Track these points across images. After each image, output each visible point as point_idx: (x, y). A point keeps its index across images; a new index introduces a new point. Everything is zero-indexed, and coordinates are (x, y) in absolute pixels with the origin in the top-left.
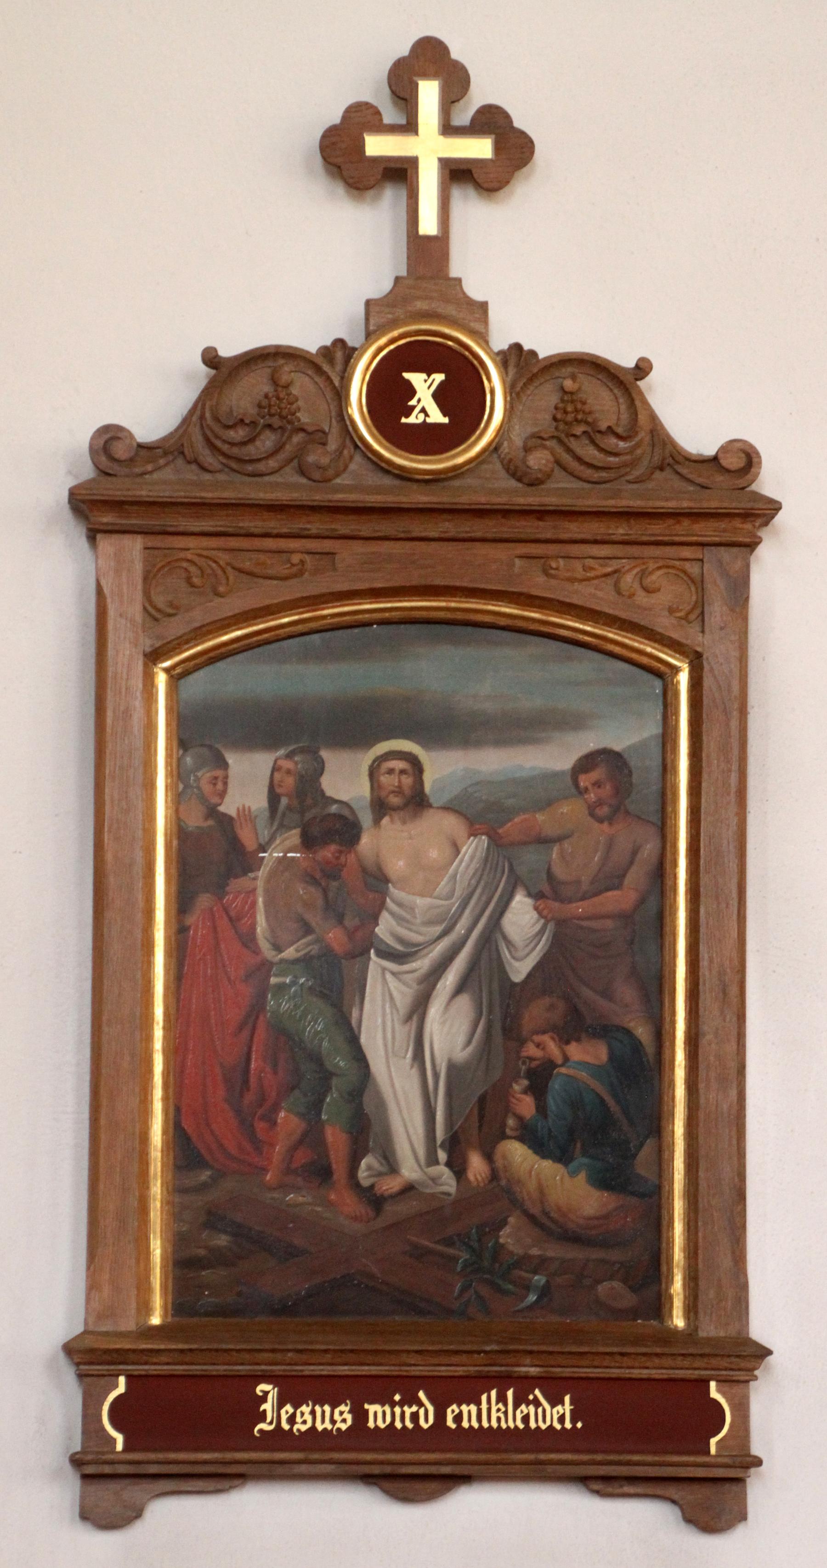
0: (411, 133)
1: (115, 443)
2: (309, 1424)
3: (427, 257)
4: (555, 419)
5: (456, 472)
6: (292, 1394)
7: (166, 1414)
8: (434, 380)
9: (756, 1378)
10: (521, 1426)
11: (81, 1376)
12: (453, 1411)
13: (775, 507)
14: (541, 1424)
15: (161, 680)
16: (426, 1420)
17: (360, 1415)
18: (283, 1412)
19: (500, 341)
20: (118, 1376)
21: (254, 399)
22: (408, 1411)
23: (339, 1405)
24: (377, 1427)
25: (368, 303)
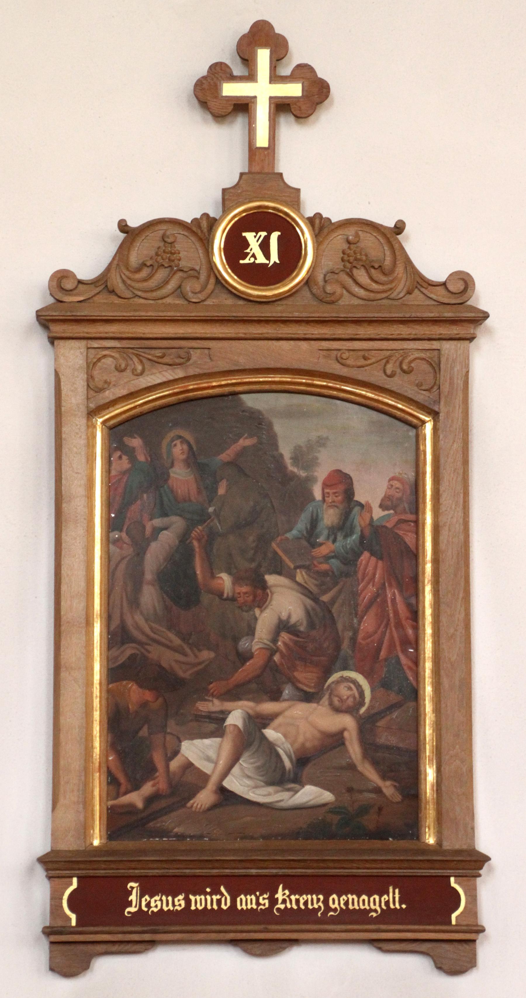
0: (253, 80)
1: (64, 281)
4: (343, 260)
6: (149, 888)
7: (99, 902)
8: (260, 236)
9: (480, 876)
10: (295, 907)
11: (49, 878)
12: (385, 899)
13: (485, 316)
16: (226, 904)
17: (188, 902)
18: (143, 900)
19: (310, 213)
20: (71, 877)
21: (152, 248)
22: (215, 898)
24: (197, 909)
25: (224, 191)
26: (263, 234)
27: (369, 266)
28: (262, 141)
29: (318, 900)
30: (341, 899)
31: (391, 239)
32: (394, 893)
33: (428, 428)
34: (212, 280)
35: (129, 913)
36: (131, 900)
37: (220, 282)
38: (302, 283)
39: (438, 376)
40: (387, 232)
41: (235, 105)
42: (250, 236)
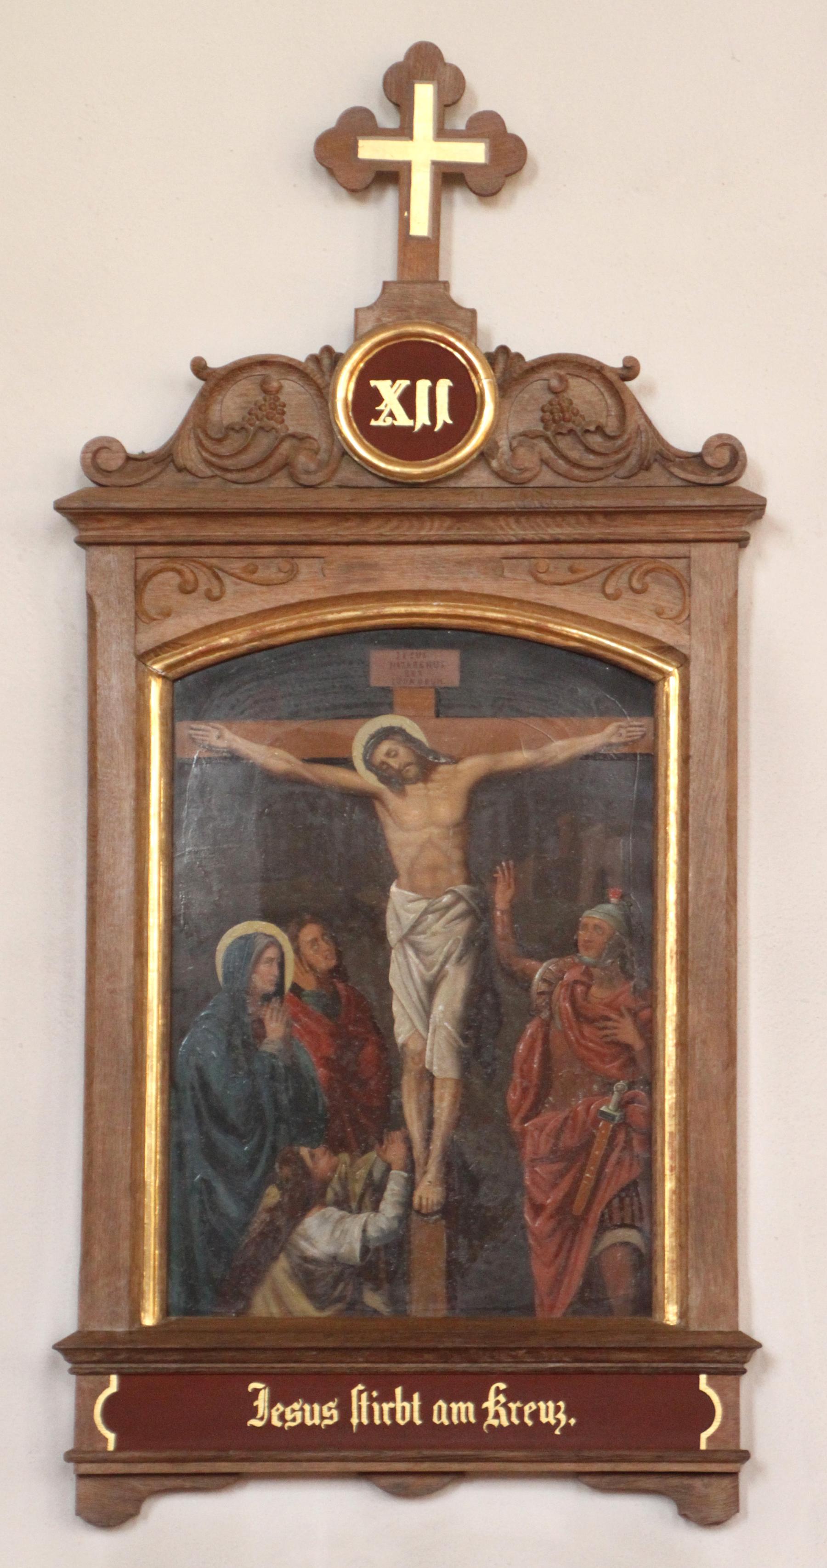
0: (412, 135)
2: (299, 1421)
3: (420, 258)
9: (744, 1372)
10: (516, 1421)
15: (156, 688)
16: (403, 1418)
17: (426, 1412)
20: (109, 1374)
21: (247, 410)
22: (386, 1407)
26: (404, 383)
27: (579, 435)
28: (420, 227)
29: (557, 1410)
32: (359, 1399)
33: (673, 686)
37: (346, 453)
38: (475, 456)
39: (687, 600)
40: (609, 375)
42: (383, 386)
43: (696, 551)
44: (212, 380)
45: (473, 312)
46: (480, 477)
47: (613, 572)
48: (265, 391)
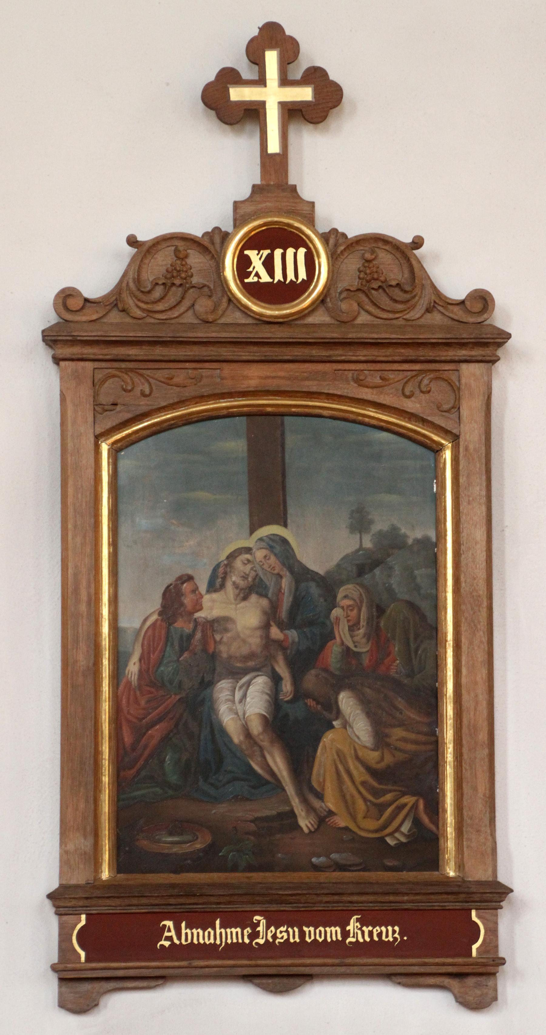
0: (274, 88)
3: (275, 167)
4: (359, 278)
5: (303, 314)
9: (501, 908)
14: (318, 937)
17: (302, 934)
19: (323, 228)
21: (169, 267)
23: (280, 927)
26: (266, 252)
28: (274, 147)
29: (394, 932)
30: (245, 931)
31: (409, 254)
33: (448, 455)
34: (225, 300)
35: (257, 943)
36: (349, 930)
37: (232, 300)
38: (318, 302)
40: (403, 248)
41: (246, 110)
42: (252, 254)
43: (464, 366)
44: (143, 250)
45: (313, 204)
46: (320, 317)
47: (409, 380)
48: (178, 258)
